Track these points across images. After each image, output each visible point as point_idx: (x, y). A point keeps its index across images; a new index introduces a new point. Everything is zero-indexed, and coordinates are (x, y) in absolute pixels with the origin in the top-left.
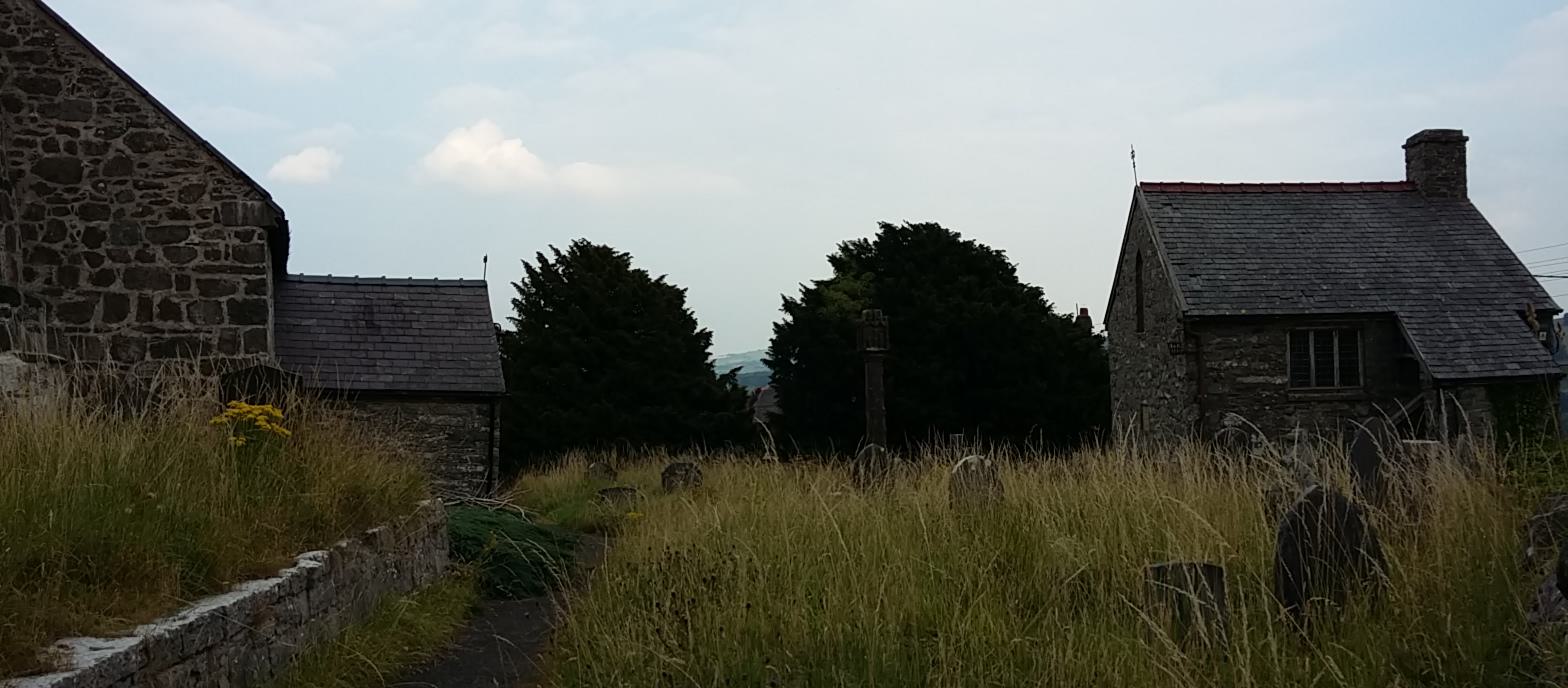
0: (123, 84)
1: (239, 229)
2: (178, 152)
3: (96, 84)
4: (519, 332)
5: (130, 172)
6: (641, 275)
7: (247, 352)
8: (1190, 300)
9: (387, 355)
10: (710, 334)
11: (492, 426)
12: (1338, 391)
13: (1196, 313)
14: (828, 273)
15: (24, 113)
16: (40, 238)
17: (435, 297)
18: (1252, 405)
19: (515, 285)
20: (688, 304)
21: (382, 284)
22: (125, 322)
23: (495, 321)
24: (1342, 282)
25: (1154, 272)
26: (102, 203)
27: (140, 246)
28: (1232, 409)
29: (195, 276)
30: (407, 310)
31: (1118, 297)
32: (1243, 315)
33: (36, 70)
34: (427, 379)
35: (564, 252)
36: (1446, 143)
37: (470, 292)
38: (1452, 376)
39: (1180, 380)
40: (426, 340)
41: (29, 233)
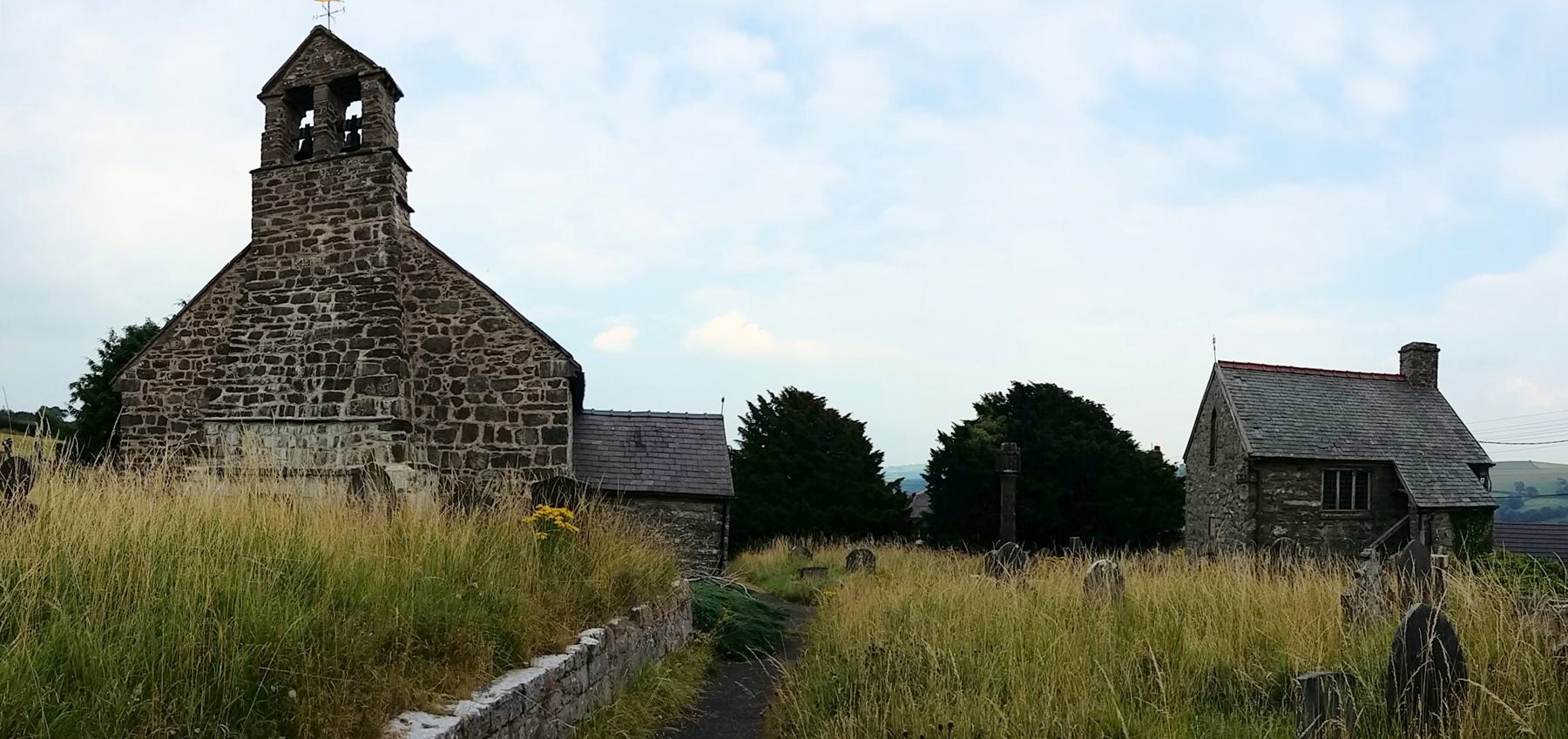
0: (479, 288)
1: (551, 379)
2: (513, 330)
3: (461, 290)
4: (742, 451)
5: (482, 344)
6: (833, 412)
7: (553, 464)
8: (1254, 445)
9: (651, 466)
10: (882, 454)
11: (724, 520)
12: (1354, 513)
13: (1258, 454)
14: (973, 415)
15: (418, 311)
16: (425, 389)
17: (686, 426)
18: (1294, 521)
19: (741, 417)
20: (867, 433)
21: (648, 416)
22: (475, 443)
23: (728, 444)
24: (1360, 438)
25: (1225, 424)
26: (463, 365)
27: (487, 392)
28: (1278, 522)
29: (521, 412)
30: (666, 434)
31: (1195, 440)
32: (1292, 458)
33: (425, 284)
34: (679, 484)
35: (776, 395)
36: (1426, 352)
37: (712, 422)
38: (1429, 505)
39: (1242, 501)
40: (679, 456)
41: (419, 386)
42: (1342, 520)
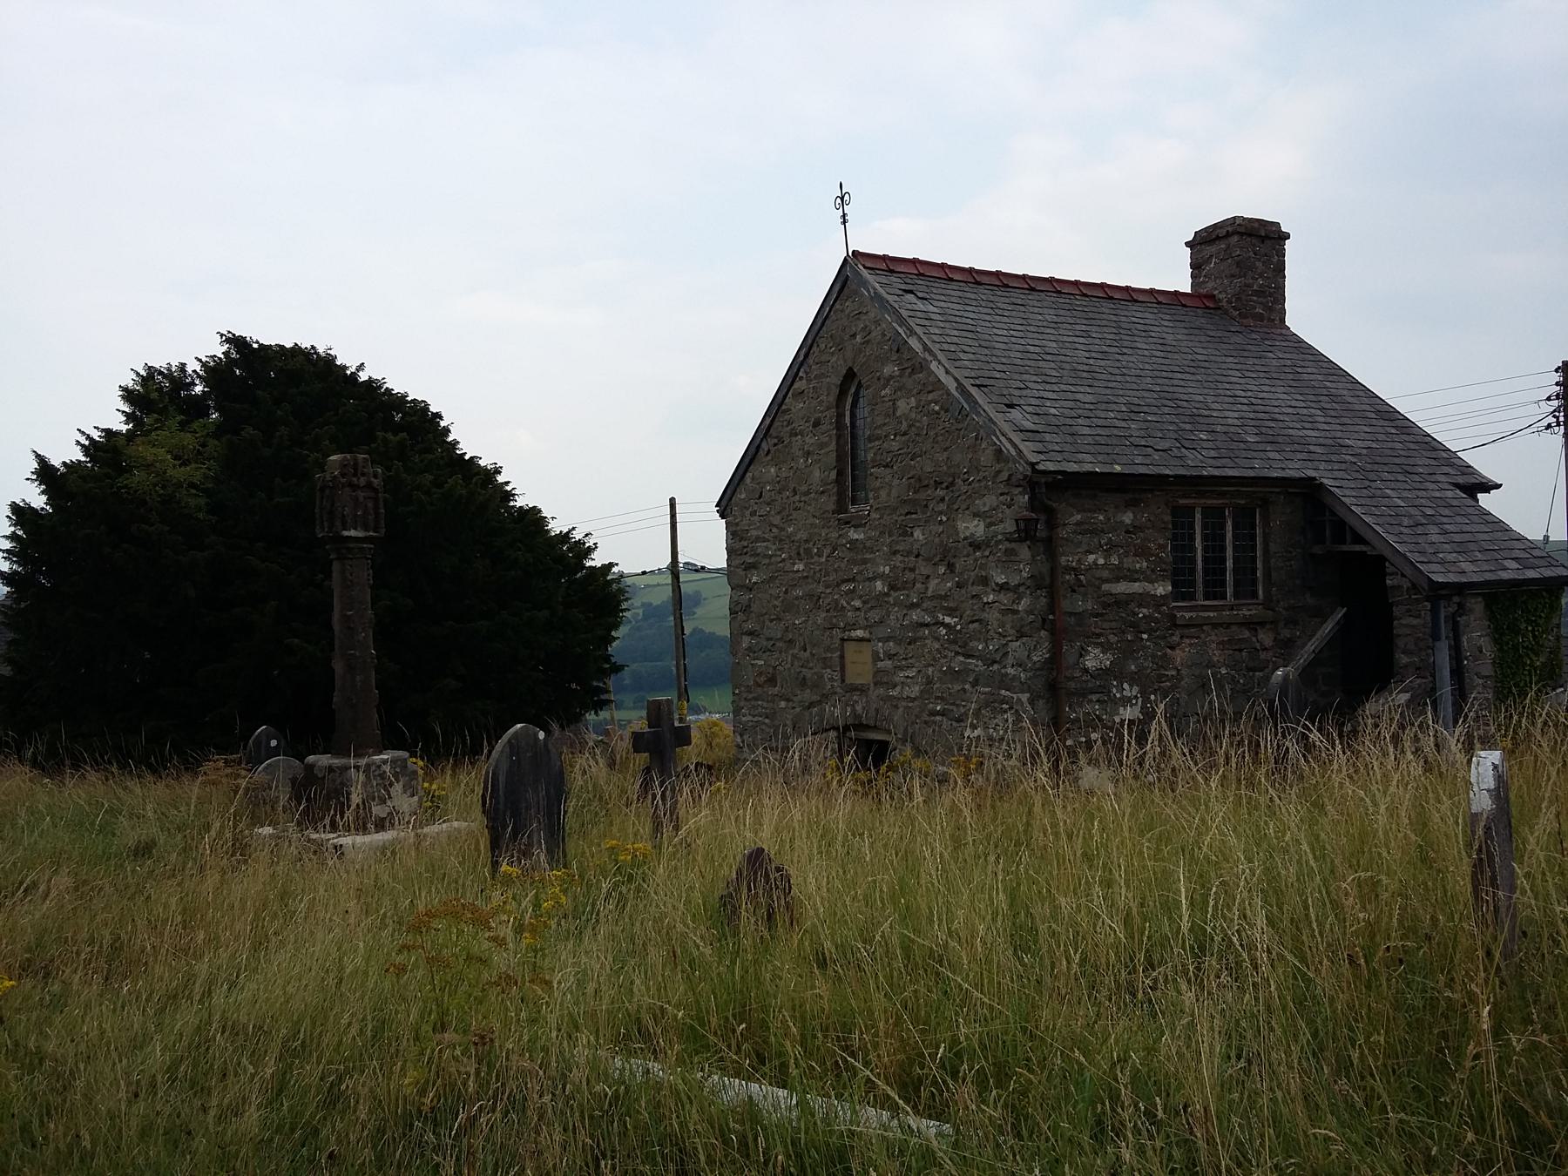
13: (1051, 467)
42: (1215, 626)
